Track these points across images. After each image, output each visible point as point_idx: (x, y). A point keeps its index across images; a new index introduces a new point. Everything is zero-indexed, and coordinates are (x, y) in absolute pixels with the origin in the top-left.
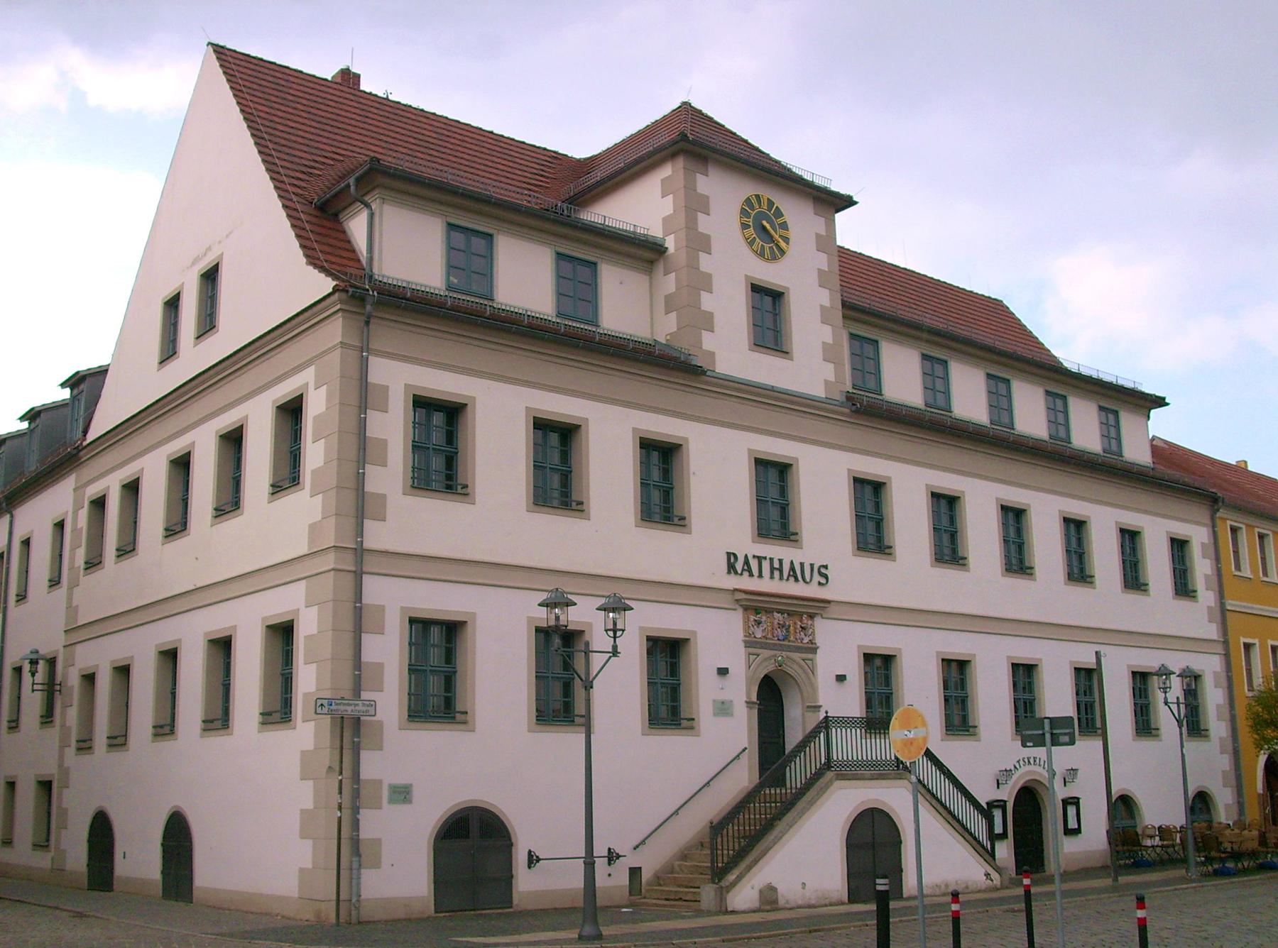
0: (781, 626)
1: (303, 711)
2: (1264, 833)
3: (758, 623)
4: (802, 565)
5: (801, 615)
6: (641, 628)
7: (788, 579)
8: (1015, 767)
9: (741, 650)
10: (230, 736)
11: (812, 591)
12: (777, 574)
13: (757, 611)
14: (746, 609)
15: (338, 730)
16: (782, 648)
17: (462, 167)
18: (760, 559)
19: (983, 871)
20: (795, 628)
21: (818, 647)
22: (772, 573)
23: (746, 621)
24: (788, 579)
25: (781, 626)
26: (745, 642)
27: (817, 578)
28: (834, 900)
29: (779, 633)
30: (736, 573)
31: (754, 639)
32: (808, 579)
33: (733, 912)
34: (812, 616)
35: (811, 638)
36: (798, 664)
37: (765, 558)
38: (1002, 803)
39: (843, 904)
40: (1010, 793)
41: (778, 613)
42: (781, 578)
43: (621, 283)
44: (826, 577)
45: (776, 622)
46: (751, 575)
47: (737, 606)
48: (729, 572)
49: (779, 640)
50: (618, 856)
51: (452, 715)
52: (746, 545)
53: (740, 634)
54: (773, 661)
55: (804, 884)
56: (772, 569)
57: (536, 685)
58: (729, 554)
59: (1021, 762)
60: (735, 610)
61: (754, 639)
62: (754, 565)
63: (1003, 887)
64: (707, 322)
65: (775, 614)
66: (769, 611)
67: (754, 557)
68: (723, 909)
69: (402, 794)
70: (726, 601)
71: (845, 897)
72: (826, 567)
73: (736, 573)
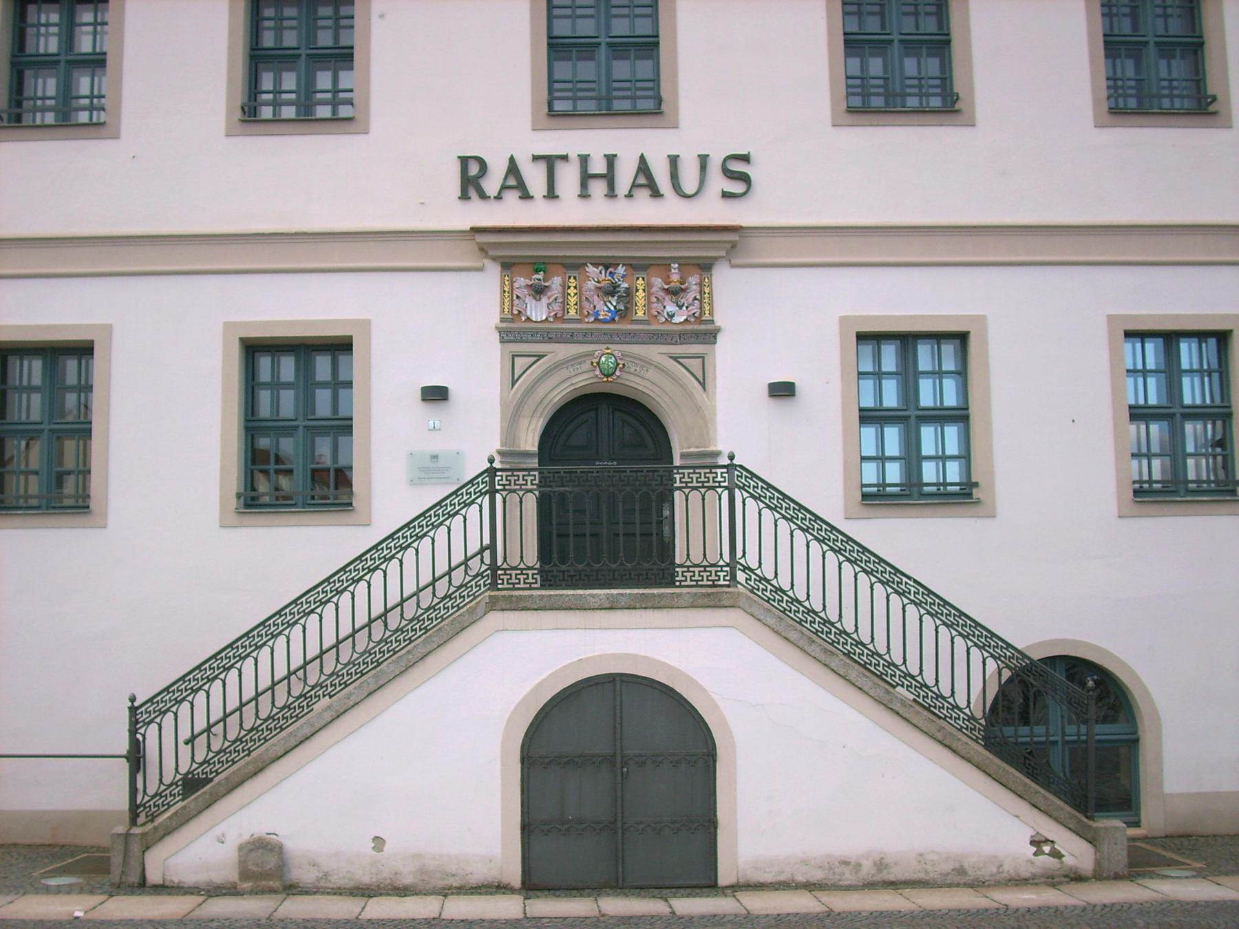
0: (611, 291)
3: (538, 291)
4: (674, 161)
5: (663, 265)
6: (228, 326)
9: (492, 353)
10: (118, 140)
12: (598, 188)
13: (539, 265)
14: (508, 266)
15: (817, 875)
16: (609, 338)
18: (550, 162)
19: (1027, 834)
20: (649, 295)
21: (718, 330)
22: (584, 185)
23: (509, 294)
25: (611, 291)
26: (501, 331)
27: (718, 183)
28: (474, 879)
29: (605, 307)
30: (483, 196)
31: (529, 325)
32: (690, 186)
33: (163, 889)
34: (705, 267)
35: (695, 309)
36: (659, 368)
37: (564, 158)
39: (500, 888)
41: (595, 265)
42: (611, 194)
44: (745, 178)
45: (591, 284)
46: (526, 196)
47: (488, 263)
48: (464, 196)
49: (597, 320)
51: (1230, 488)
53: (493, 316)
54: (587, 366)
55: (376, 839)
56: (586, 177)
58: (464, 161)
60: (480, 269)
61: (529, 325)
62: (535, 178)
63: (1100, 875)
65: (591, 269)
66: (575, 266)
67: (536, 158)
68: (134, 878)
70: (465, 255)
71: (514, 875)
72: (745, 159)
73: (483, 196)
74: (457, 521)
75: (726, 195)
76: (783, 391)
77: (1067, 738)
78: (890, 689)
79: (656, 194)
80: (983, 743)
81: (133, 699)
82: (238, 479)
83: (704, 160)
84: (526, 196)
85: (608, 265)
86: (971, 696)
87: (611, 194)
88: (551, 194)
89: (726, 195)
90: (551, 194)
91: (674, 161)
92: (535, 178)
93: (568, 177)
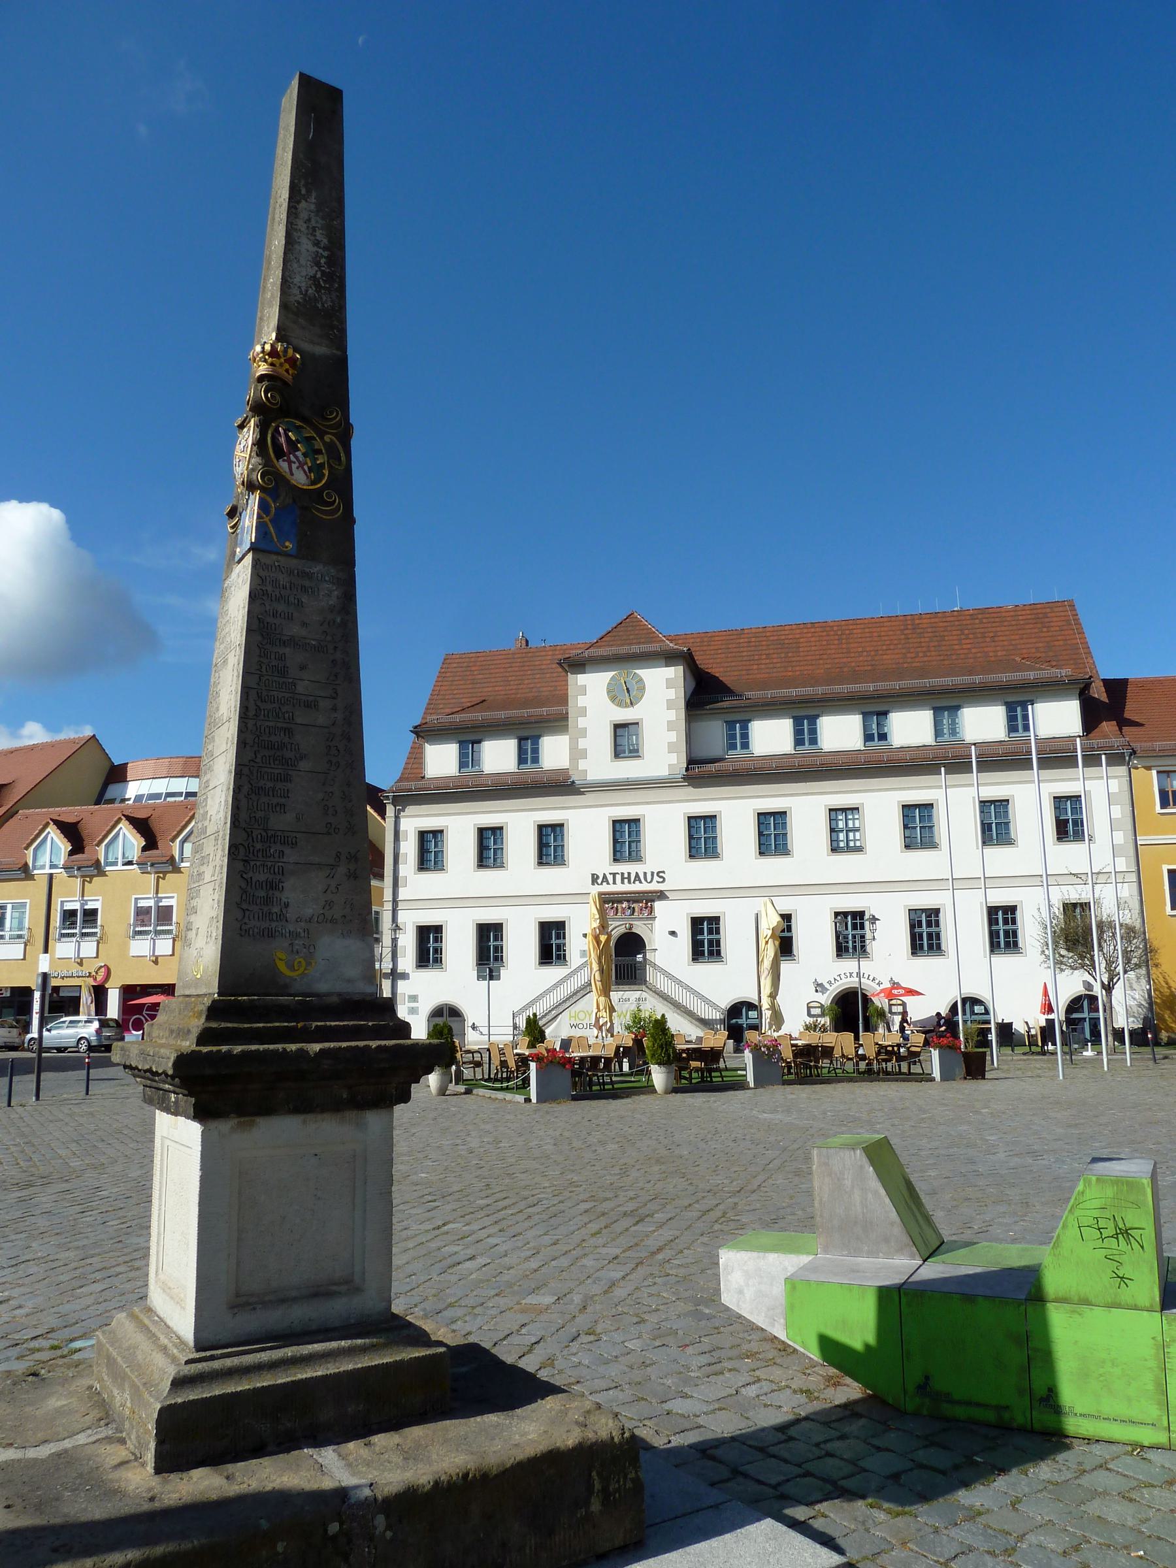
1: (1165, 894)
2: (172, 1032)
4: (645, 874)
7: (634, 883)
8: (835, 979)
11: (654, 886)
17: (489, 658)
18: (614, 875)
24: (634, 883)
27: (656, 878)
32: (649, 880)
38: (968, 1006)
40: (827, 999)
42: (629, 882)
43: (8, 1507)
44: (664, 879)
46: (608, 884)
50: (332, 709)
52: (603, 862)
56: (623, 879)
57: (328, 84)
59: (843, 976)
62: (610, 878)
64: (583, 754)
67: (610, 874)
69: (414, 998)
72: (663, 872)
74: (582, 971)
75: (658, 882)
76: (673, 933)
77: (792, 1042)
78: (1022, 656)
79: (641, 882)
80: (253, 541)
81: (911, 992)
82: (382, 922)
83: (652, 873)
84: (608, 884)
85: (628, 901)
86: (1107, 1164)
87: (622, 874)
88: (614, 883)
89: (658, 882)
90: (614, 883)
91: (645, 874)
92: (610, 878)
93: (618, 877)
